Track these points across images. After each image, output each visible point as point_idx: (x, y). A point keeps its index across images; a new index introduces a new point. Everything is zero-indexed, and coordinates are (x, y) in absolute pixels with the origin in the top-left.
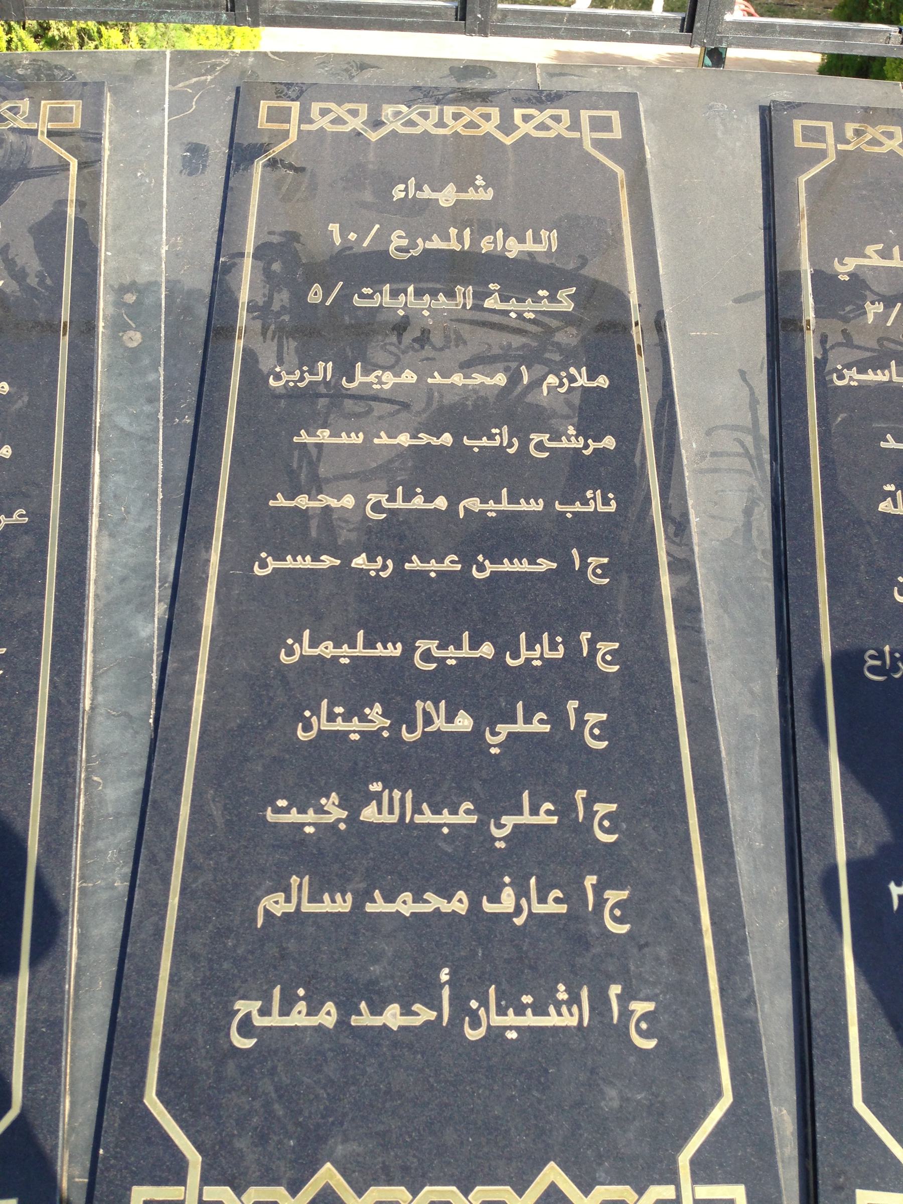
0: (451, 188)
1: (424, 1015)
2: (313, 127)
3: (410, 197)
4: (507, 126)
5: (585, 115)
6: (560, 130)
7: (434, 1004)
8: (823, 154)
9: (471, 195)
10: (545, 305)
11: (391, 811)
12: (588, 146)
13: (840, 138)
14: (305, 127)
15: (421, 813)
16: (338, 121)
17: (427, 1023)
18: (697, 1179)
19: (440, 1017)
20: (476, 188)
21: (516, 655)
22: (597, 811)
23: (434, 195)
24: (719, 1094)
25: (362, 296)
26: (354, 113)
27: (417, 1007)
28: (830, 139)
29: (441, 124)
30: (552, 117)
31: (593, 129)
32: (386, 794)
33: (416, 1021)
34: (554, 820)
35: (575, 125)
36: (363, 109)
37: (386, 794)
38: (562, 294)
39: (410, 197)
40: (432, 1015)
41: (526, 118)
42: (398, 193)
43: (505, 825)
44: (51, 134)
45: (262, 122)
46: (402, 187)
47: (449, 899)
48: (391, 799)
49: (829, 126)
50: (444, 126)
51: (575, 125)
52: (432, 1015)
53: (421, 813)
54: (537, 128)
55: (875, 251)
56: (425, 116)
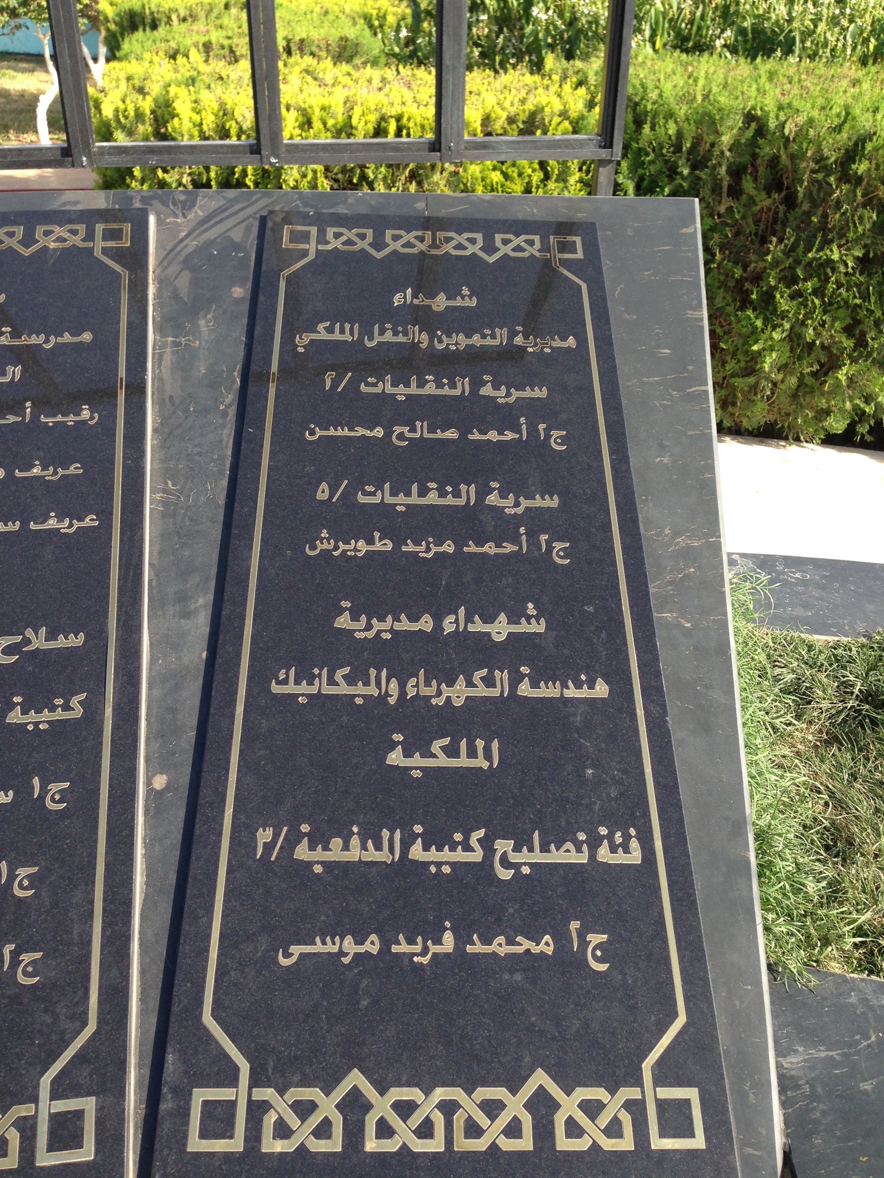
2: (329, 247)
3: (408, 303)
4: (490, 248)
6: (76, 241)
8: (305, 253)
9: (459, 302)
10: (59, 715)
12: (98, 253)
13: (322, 239)
15: (473, 622)
16: (460, 247)
18: (659, 1081)
23: (427, 302)
24: (675, 1015)
25: (368, 384)
26: (473, 241)
30: (468, 239)
31: (104, 239)
35: (90, 236)
38: (75, 701)
39: (408, 303)
42: (397, 299)
44: (105, 251)
45: (285, 243)
49: (314, 230)
53: (473, 622)
54: (514, 250)
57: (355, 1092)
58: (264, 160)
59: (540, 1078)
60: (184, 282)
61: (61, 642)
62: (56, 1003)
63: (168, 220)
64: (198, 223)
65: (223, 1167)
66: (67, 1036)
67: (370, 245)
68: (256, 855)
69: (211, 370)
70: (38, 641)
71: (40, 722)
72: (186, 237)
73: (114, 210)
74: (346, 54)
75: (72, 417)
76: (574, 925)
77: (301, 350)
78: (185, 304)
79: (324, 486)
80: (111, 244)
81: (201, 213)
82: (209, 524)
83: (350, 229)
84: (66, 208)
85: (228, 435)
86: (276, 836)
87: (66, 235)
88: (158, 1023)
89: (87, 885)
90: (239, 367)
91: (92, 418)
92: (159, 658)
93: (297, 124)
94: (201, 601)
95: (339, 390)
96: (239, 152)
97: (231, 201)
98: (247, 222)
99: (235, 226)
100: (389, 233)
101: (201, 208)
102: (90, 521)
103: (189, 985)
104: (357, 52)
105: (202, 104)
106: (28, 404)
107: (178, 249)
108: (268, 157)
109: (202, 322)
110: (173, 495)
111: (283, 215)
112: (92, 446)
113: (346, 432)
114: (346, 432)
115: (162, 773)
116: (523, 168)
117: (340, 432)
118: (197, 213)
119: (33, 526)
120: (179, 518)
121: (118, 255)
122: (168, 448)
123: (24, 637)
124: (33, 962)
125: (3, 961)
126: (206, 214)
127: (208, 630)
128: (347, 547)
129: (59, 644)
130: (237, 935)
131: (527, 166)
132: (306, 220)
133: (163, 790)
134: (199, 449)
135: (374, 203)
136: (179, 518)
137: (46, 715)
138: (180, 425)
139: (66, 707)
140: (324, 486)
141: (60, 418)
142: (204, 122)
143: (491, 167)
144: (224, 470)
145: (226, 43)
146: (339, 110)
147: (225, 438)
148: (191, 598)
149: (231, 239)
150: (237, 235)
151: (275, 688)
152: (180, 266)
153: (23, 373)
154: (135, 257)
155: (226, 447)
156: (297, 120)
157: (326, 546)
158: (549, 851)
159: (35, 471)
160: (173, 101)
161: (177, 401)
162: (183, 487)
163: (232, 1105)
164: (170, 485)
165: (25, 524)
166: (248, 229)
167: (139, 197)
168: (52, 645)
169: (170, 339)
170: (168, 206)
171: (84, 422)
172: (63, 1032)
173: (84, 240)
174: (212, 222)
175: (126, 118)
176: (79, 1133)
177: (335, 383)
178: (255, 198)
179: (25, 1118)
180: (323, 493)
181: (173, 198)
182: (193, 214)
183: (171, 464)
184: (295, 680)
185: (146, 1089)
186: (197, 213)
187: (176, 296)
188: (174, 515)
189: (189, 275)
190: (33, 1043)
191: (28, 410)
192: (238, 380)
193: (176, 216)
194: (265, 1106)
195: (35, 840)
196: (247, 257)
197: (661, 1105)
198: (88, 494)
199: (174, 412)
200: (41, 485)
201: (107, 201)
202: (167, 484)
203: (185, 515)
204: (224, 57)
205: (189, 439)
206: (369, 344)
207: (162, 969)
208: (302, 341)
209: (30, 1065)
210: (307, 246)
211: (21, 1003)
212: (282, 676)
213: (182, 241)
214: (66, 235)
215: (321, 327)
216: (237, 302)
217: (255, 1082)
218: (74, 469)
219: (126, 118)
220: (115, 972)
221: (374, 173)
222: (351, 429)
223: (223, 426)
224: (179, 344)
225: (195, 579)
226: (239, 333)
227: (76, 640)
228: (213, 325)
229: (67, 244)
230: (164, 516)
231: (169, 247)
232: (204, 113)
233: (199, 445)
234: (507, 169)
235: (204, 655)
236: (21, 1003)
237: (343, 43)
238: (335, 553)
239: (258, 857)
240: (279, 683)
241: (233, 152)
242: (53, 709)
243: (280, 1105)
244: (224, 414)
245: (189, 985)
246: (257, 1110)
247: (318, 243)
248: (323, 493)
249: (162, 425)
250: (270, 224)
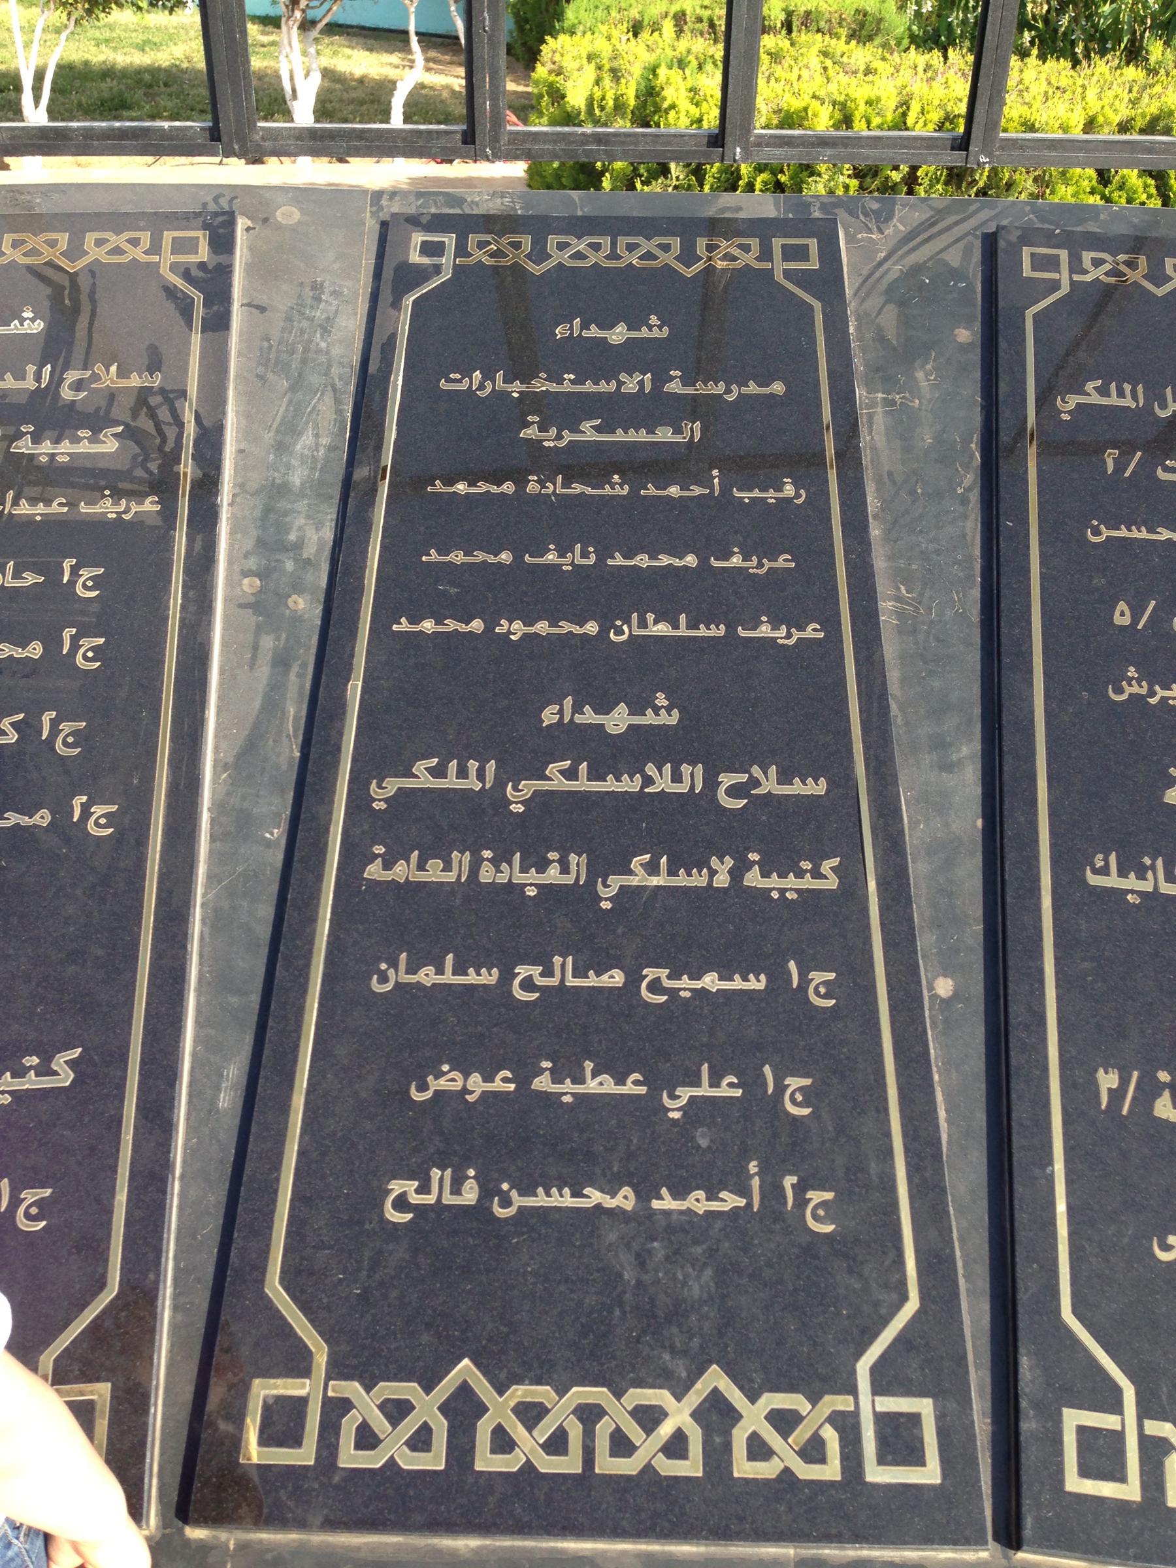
0: (621, 328)
1: (730, 1201)
2: (1088, 278)
5: (777, 243)
6: (749, 259)
7: (743, 1190)
8: (1055, 286)
12: (778, 276)
13: (1076, 266)
17: (736, 1209)
19: (749, 1205)
20: (650, 328)
22: (789, 1085)
26: (666, 248)
27: (723, 1195)
29: (614, 256)
33: (725, 1207)
34: (738, 1093)
35: (766, 254)
36: (676, 243)
40: (742, 1202)
41: (99, 243)
43: (679, 1097)
47: (613, 1194)
49: (1064, 254)
51: (155, 249)
52: (742, 1202)
57: (464, 1390)
58: (971, 158)
60: (889, 318)
61: (797, 788)
62: (862, 1263)
63: (859, 236)
64: (899, 241)
65: (1118, 1519)
66: (883, 1311)
68: (1099, 1104)
69: (939, 439)
70: (770, 784)
71: (786, 890)
72: (886, 259)
73: (785, 220)
74: (864, 33)
75: (771, 493)
77: (1066, 417)
78: (895, 349)
79: (1122, 606)
80: (792, 265)
81: (902, 228)
82: (962, 648)
84: (726, 215)
85: (972, 527)
86: (1124, 1082)
87: (736, 252)
88: (992, 1308)
89: (878, 1111)
90: (976, 437)
91: (798, 496)
92: (918, 822)
93: (831, 123)
94: (965, 750)
95: (1127, 475)
96: (937, 147)
97: (939, 211)
98: (965, 241)
99: (949, 246)
101: (901, 220)
102: (812, 631)
103: (1035, 1266)
104: (879, 29)
105: (701, 93)
106: (715, 472)
107: (877, 275)
108: (977, 154)
109: (920, 375)
110: (908, 604)
111: (1019, 233)
112: (799, 531)
113: (1144, 534)
114: (1144, 534)
115: (945, 976)
116: (1135, 192)
117: (1135, 534)
118: (897, 227)
119: (742, 633)
120: (921, 637)
121: (803, 279)
122: (895, 542)
123: (751, 776)
124: (823, 1204)
125: (785, 1198)
126: (909, 228)
127: (979, 790)
128: (1167, 693)
129: (795, 790)
130: (1091, 1210)
131: (1141, 190)
132: (1050, 239)
133: (950, 999)
134: (936, 546)
135: (1136, 221)
136: (921, 637)
137: (791, 882)
138: (907, 512)
139: (817, 874)
140: (1122, 606)
141: (756, 493)
142: (705, 118)
143: (1088, 190)
144: (974, 576)
145: (706, 14)
146: (890, 104)
147: (968, 531)
148: (951, 745)
149: (946, 264)
150: (954, 258)
151: (1093, 880)
152: (883, 299)
153: (704, 430)
154: (828, 282)
155: (973, 545)
156: (831, 118)
157: (1135, 689)
159: (735, 560)
160: (663, 89)
161: (899, 479)
162: (921, 595)
164: (904, 592)
165: (731, 629)
166: (968, 251)
167: (818, 204)
168: (786, 790)
169: (880, 395)
170: (858, 217)
171: (788, 501)
172: (876, 1304)
173: (758, 259)
174: (919, 240)
175: (602, 108)
176: (918, 1445)
177: (1120, 467)
178: (972, 208)
179: (843, 1412)
180: (1122, 616)
181: (864, 207)
182: (892, 229)
183: (902, 563)
184: (1118, 870)
185: (989, 1397)
186: (897, 227)
187: (881, 338)
188: (914, 631)
189: (896, 310)
190: (838, 1314)
191: (716, 480)
192: (978, 455)
193: (870, 231)
195: (802, 1043)
196: (970, 287)
197: (882, 1419)
198: (802, 596)
199: (897, 493)
200: (745, 579)
201: (778, 209)
202: (898, 589)
203: (928, 632)
204: (702, 34)
205: (921, 531)
206: (1164, 414)
207: (987, 1239)
208: (1068, 404)
209: (840, 1342)
210: (1056, 276)
211: (816, 1257)
212: (1099, 864)
213: (881, 264)
214: (736, 252)
215: (1090, 386)
216: (964, 348)
218: (783, 562)
219: (602, 108)
220: (933, 1233)
221: (926, 192)
222: (1151, 530)
223: (965, 516)
224: (893, 403)
225: (952, 721)
226: (971, 390)
227: (817, 788)
228: (935, 379)
229: (738, 264)
230: (900, 633)
231: (865, 272)
232: (705, 105)
233: (935, 540)
234: (1111, 193)
235: (979, 823)
236: (816, 1257)
237: (861, 17)
238: (1153, 701)
239: (1103, 1107)
240: (1096, 871)
241: (928, 147)
242: (800, 874)
243: (366, 1403)
244: (964, 501)
245: (1035, 1266)
246: (336, 1409)
247: (1072, 271)
248: (1122, 616)
249: (883, 510)
250: (1002, 244)
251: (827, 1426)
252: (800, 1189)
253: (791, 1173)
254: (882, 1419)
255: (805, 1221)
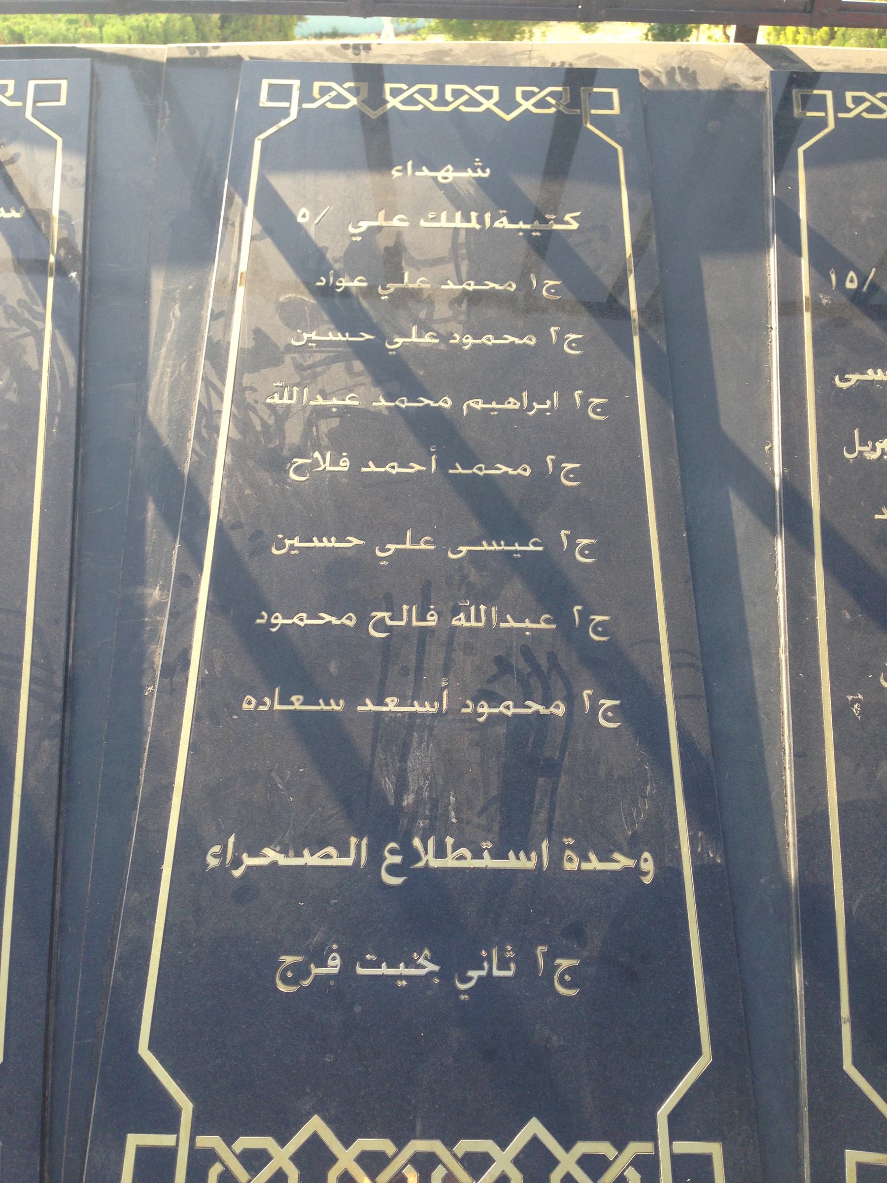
4: (508, 103)
11: (478, 619)
13: (306, 95)
14: (305, 106)
16: (410, 101)
21: (851, 450)
24: (698, 1053)
26: (488, 95)
28: (296, 94)
29: (441, 101)
32: (473, 609)
37: (473, 609)
45: (264, 101)
46: (399, 168)
48: (478, 611)
49: (296, 83)
50: (447, 104)
51: (20, 94)
55: (572, 217)
56: (426, 94)
57: (315, 1140)
59: (316, 1125)
67: (496, 104)
76: (541, 950)
83: (873, 93)
100: (519, 90)
158: (302, 856)
163: (170, 1154)
194: (211, 1156)
197: (677, 1160)
217: (198, 1129)
251: (631, 1169)
252: (550, 957)
253: (542, 944)
254: (677, 1160)
255: (554, 987)
